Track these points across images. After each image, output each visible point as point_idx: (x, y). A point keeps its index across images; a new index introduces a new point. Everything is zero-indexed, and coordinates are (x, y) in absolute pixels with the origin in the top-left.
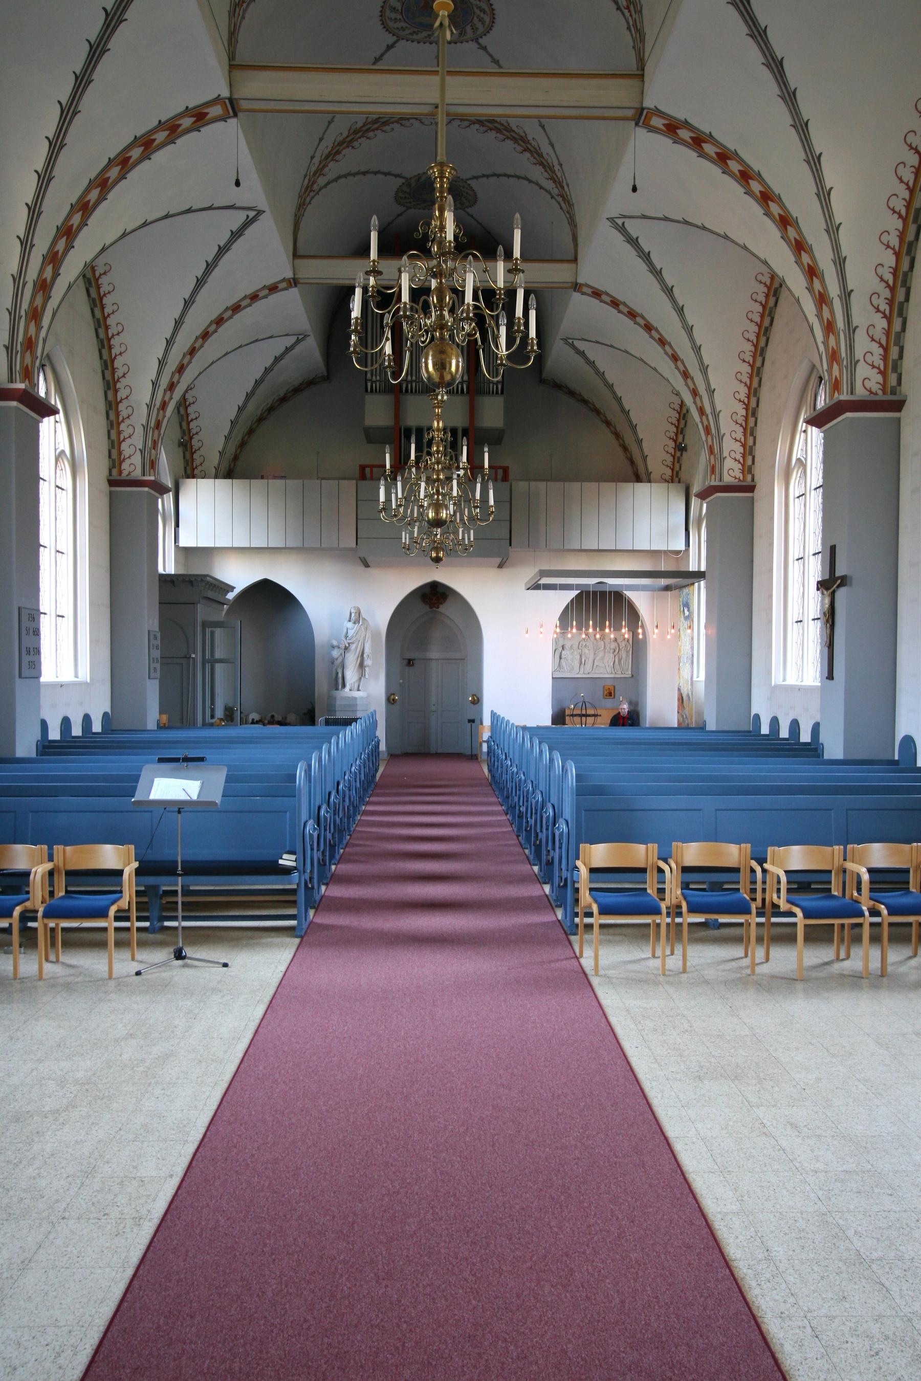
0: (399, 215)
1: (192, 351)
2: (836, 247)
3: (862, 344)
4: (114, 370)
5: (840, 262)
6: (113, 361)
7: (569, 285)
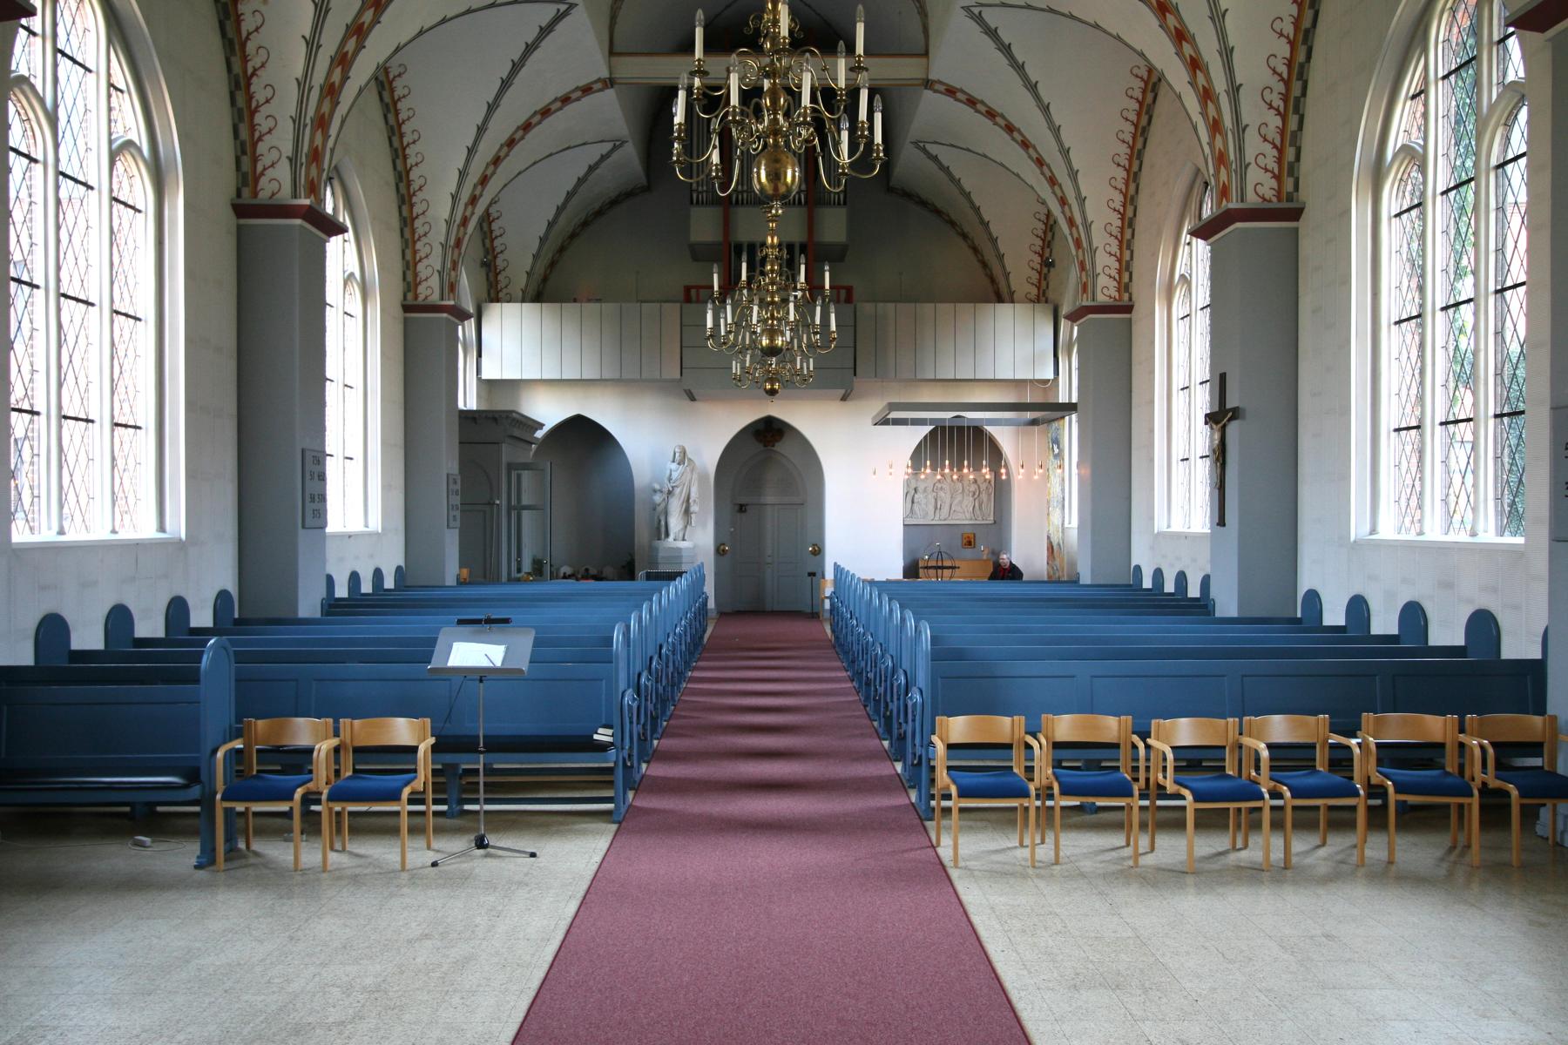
1: (497, 161)
2: (1222, 35)
3: (1253, 145)
5: (1227, 53)
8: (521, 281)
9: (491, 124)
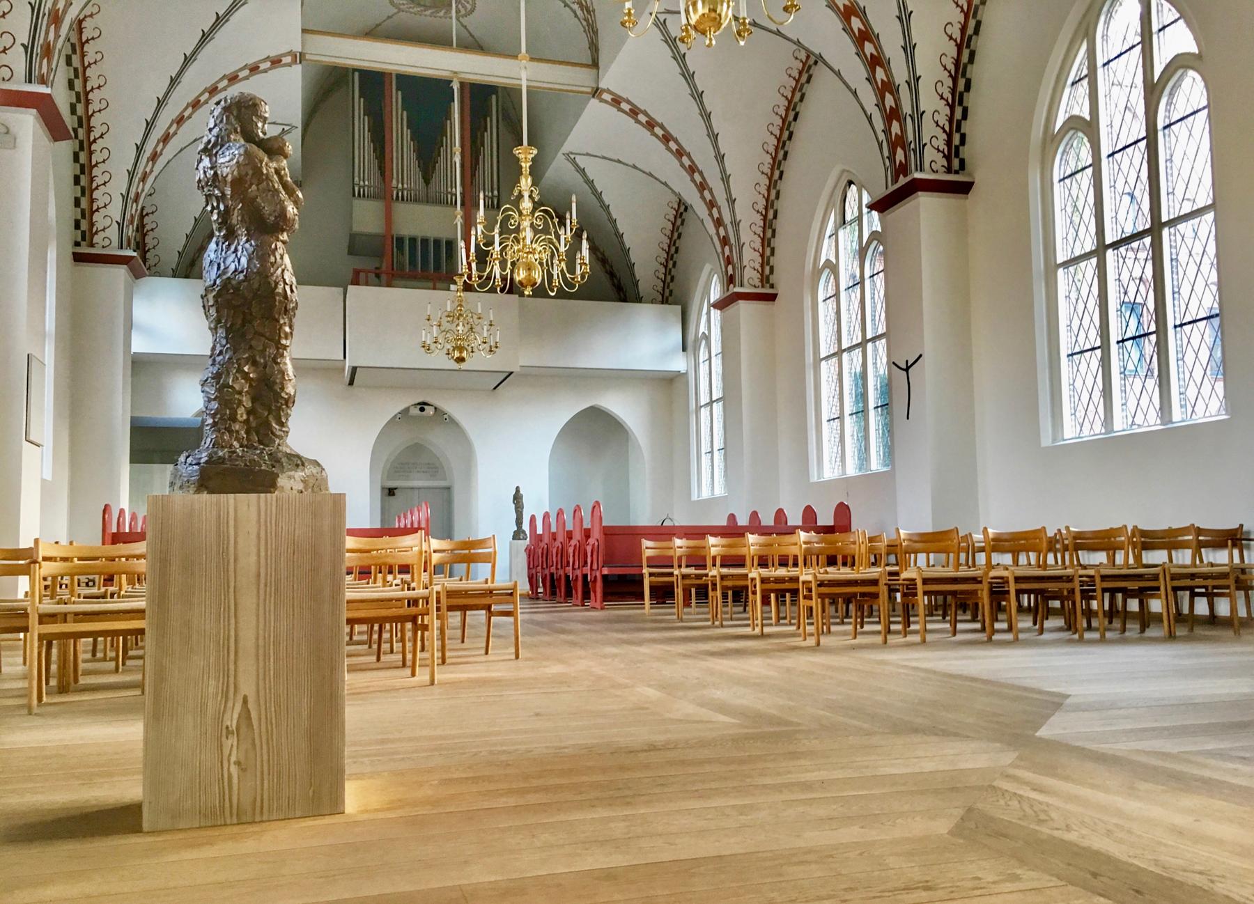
0: (389, 17)
1: (180, 120)
3: (929, 129)
4: (90, 130)
5: (909, 49)
6: (89, 118)
7: (589, 90)
8: (172, 259)
9: (201, 56)
